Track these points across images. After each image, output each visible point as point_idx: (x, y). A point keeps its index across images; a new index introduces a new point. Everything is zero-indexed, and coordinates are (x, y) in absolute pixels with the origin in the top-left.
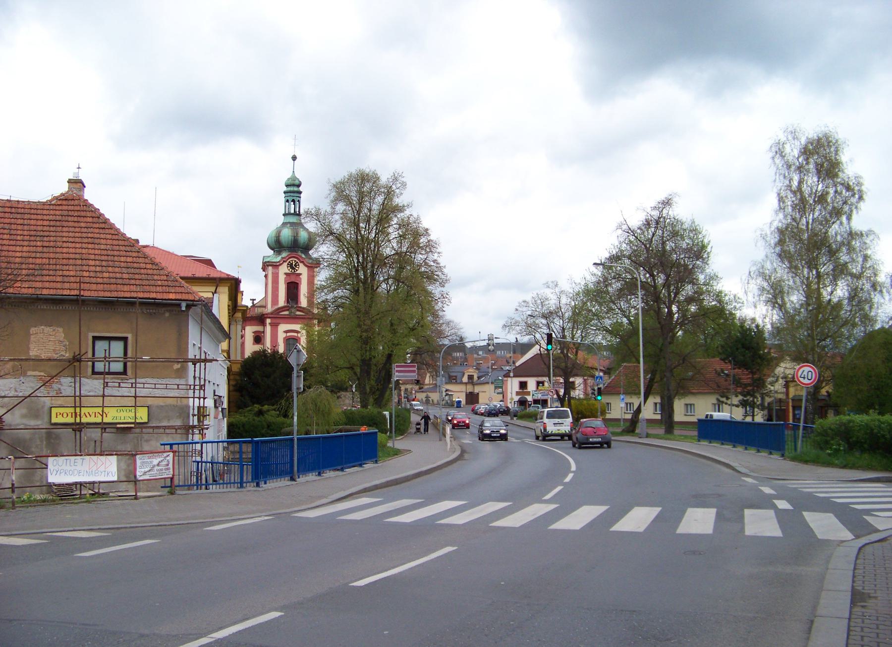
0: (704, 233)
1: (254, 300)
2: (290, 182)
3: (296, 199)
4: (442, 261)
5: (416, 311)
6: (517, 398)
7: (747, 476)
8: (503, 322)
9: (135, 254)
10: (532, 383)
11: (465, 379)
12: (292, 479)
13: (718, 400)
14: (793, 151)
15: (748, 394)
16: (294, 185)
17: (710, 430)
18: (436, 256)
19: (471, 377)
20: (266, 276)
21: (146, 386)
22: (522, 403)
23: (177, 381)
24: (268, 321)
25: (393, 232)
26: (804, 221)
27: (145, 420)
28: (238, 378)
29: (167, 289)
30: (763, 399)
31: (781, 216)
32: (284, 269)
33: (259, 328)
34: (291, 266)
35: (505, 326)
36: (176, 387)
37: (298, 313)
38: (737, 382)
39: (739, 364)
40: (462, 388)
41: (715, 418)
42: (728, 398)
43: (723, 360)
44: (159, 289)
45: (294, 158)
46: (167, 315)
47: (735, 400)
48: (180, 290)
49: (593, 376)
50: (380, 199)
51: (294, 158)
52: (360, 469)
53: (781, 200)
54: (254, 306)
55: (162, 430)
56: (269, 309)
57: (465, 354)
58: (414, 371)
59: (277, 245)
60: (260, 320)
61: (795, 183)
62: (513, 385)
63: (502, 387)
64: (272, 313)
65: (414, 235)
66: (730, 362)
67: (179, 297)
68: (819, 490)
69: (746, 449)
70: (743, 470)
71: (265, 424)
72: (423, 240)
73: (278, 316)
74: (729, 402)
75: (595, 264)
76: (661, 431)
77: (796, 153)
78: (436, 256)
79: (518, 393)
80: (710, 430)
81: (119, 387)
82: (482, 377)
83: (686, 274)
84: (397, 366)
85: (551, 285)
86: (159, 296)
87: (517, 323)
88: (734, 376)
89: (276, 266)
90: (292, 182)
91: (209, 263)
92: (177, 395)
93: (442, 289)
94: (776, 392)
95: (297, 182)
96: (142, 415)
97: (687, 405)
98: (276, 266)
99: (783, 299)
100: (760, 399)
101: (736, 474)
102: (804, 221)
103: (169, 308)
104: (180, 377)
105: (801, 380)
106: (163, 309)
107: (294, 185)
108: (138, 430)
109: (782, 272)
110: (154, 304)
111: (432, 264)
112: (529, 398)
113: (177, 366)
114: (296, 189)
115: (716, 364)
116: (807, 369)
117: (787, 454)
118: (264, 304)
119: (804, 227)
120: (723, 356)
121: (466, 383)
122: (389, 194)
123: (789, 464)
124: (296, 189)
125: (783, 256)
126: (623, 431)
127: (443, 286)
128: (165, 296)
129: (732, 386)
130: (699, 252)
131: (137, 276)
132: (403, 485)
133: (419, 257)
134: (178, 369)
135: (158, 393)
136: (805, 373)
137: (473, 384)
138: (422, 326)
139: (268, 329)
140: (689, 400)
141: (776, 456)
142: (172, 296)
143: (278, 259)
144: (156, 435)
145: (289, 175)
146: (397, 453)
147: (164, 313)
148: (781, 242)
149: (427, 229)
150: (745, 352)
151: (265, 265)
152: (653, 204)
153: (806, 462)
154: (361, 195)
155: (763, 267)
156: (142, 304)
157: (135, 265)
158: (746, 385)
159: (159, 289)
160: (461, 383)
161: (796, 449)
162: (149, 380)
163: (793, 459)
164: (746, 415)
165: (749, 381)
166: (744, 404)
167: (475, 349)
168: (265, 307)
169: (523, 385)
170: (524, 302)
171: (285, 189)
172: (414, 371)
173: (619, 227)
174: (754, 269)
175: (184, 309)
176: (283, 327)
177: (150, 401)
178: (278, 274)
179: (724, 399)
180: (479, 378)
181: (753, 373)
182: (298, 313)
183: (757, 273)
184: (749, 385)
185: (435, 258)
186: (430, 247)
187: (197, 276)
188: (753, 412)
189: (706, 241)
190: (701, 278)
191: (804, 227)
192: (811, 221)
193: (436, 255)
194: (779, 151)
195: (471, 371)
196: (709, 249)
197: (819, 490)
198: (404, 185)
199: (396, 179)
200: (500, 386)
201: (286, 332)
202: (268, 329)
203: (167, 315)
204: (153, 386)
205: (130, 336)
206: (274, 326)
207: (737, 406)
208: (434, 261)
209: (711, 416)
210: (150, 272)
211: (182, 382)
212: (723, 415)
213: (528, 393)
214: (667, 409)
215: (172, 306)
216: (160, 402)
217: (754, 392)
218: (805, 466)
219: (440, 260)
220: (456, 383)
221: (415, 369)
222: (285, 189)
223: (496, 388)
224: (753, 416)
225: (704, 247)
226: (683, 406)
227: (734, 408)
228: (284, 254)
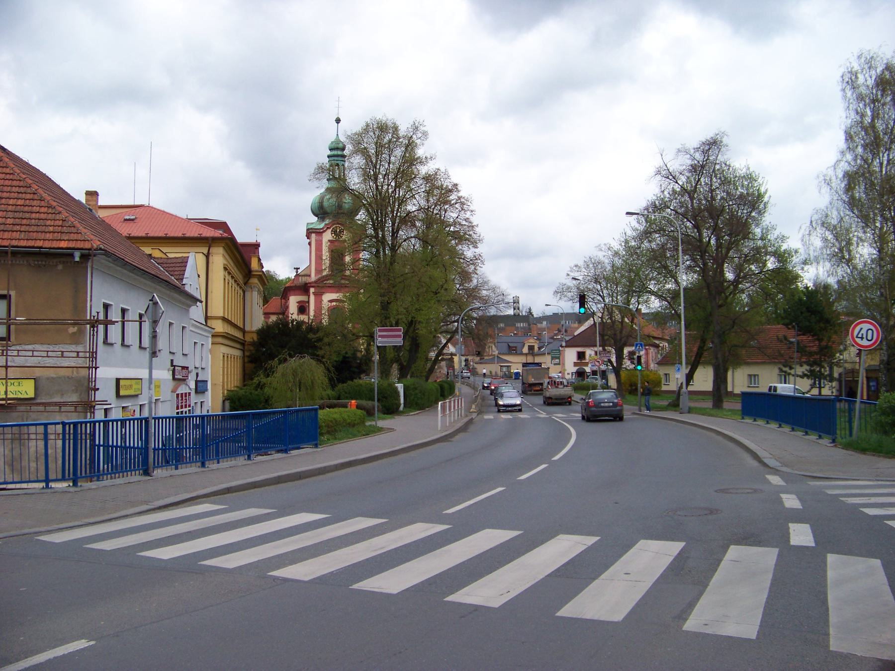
0: (760, 180)
1: (297, 269)
2: (334, 146)
3: (341, 163)
4: (475, 220)
5: (437, 273)
6: (575, 369)
7: (775, 471)
8: (554, 289)
9: (31, 196)
10: (589, 352)
11: (525, 350)
12: (146, 473)
13: (781, 370)
14: (866, 80)
15: (815, 363)
16: (337, 149)
17: (761, 406)
18: (468, 214)
19: (531, 348)
20: (310, 244)
21: (36, 353)
22: (581, 374)
23: (73, 348)
24: (312, 290)
25: (419, 186)
26: (876, 162)
27: (31, 394)
28: (252, 348)
29: (58, 236)
30: (831, 369)
31: (849, 157)
32: (328, 236)
33: (303, 298)
34: (334, 232)
35: (556, 292)
36: (75, 354)
37: (343, 282)
38: (801, 349)
39: (804, 330)
40: (523, 359)
41: (779, 392)
42: (791, 368)
43: (786, 325)
44: (48, 236)
45: (338, 121)
46: (60, 267)
47: (800, 370)
48: (75, 237)
49: (657, 346)
50: (398, 152)
51: (338, 121)
52: (284, 455)
53: (849, 137)
54: (297, 275)
55: (41, 408)
56: (313, 278)
57: (529, 325)
58: (399, 336)
59: (320, 211)
60: (304, 289)
61: (868, 119)
62: (570, 355)
63: (559, 358)
64: (316, 282)
65: (441, 193)
66: (793, 327)
67: (72, 245)
68: (873, 500)
69: (793, 429)
70: (772, 463)
71: (262, 399)
72: (453, 197)
73: (321, 286)
74: (792, 372)
75: (628, 213)
76: (708, 404)
77: (871, 82)
78: (468, 214)
79: (575, 364)
80: (761, 406)
81: (62, 356)
82: (542, 347)
83: (740, 229)
84: (380, 330)
85: (603, 248)
86: (47, 244)
87: (569, 289)
88: (798, 343)
89: (319, 233)
90: (336, 146)
91: (223, 226)
92: (73, 364)
93: (476, 250)
94: (846, 362)
95: (341, 145)
96: (27, 389)
97: (750, 376)
98: (319, 233)
99: (849, 252)
100: (828, 369)
101: (762, 468)
102: (876, 162)
103: (62, 259)
104: (77, 343)
105: (858, 340)
106: (55, 261)
107: (337, 149)
108: (22, 408)
109: (851, 219)
110: (40, 254)
111: (464, 223)
112: (588, 369)
113: (73, 330)
114: (339, 153)
115: (779, 330)
116: (866, 326)
117: (839, 439)
118: (307, 272)
119: (877, 169)
120: (787, 321)
121: (526, 354)
122: (410, 146)
123: (839, 453)
124: (339, 153)
125: (852, 203)
126: (669, 405)
127: (477, 247)
128: (55, 244)
129: (795, 355)
130: (754, 201)
131: (24, 222)
132: (304, 481)
133: (452, 215)
134: (74, 333)
135: (50, 362)
136: (864, 332)
137: (533, 355)
138: (446, 289)
139: (312, 298)
140: (753, 370)
141: (826, 441)
142: (63, 244)
143: (322, 226)
144: (46, 414)
145: (333, 138)
146: (380, 430)
147: (56, 265)
148: (849, 189)
149: (456, 185)
150: (811, 319)
151: (310, 232)
152: (696, 145)
153: (863, 451)
154: (379, 146)
155: (827, 216)
156: (14, 254)
157: (26, 209)
158: (811, 354)
159: (48, 236)
160: (522, 354)
161: (851, 435)
162: (38, 347)
163: (848, 446)
164: (813, 386)
165: (815, 349)
166: (812, 375)
167: (541, 319)
168: (309, 276)
169: (581, 356)
170: (576, 266)
171: (329, 153)
172: (399, 336)
173: (658, 172)
174: (815, 217)
175: (77, 259)
176: (327, 297)
177: (38, 373)
178: (321, 241)
179: (787, 369)
180: (539, 348)
181: (820, 340)
182: (343, 282)
183: (819, 222)
184: (816, 353)
185: (467, 216)
186: (462, 203)
187: (187, 235)
188: (820, 384)
189: (762, 190)
190: (758, 231)
191: (877, 169)
192: (885, 162)
193: (468, 213)
194: (851, 80)
195: (532, 341)
196: (766, 199)
197: (873, 500)
198: (425, 134)
199: (416, 129)
200: (557, 357)
201: (331, 301)
202: (312, 298)
203: (60, 267)
204: (45, 354)
205: (13, 293)
206: (318, 295)
207: (802, 377)
208: (466, 220)
209: (775, 389)
210: (42, 216)
211: (80, 348)
212: (785, 389)
213: (586, 364)
214: (720, 380)
215: (65, 256)
216: (51, 373)
217: (821, 361)
218: (862, 456)
219: (472, 219)
220: (516, 354)
221: (401, 333)
222: (329, 153)
223: (553, 358)
224: (820, 388)
225: (760, 196)
226: (746, 377)
227: (798, 379)
228: (327, 221)
